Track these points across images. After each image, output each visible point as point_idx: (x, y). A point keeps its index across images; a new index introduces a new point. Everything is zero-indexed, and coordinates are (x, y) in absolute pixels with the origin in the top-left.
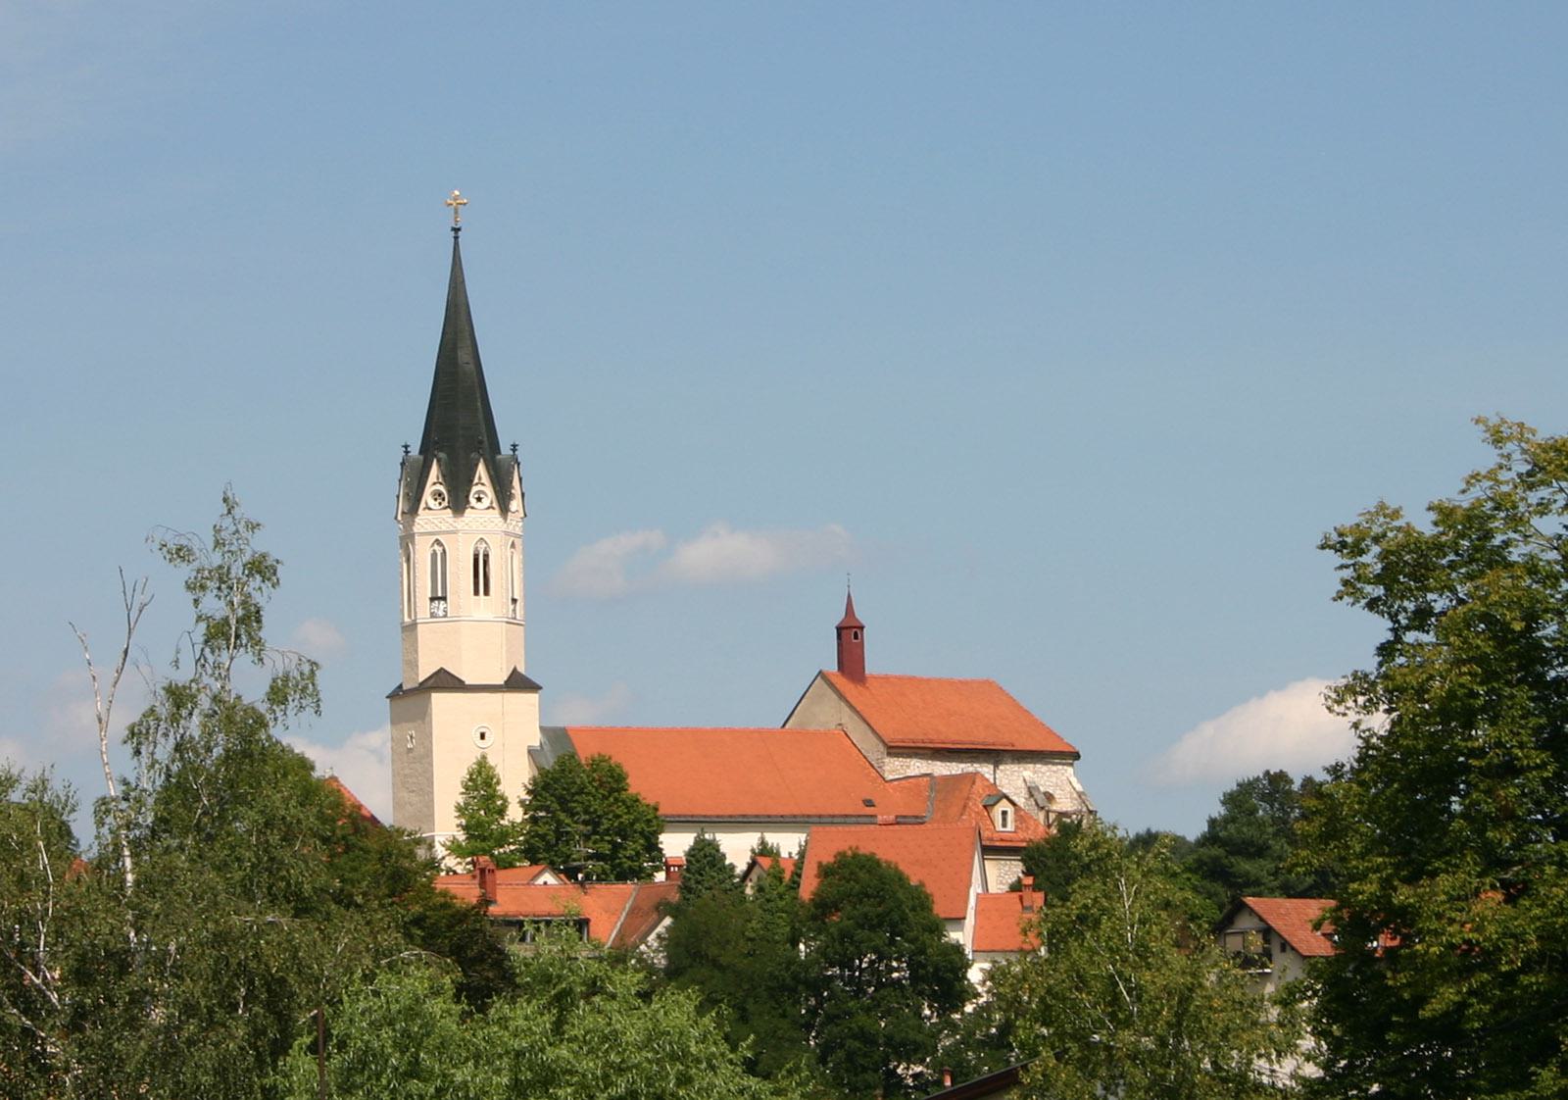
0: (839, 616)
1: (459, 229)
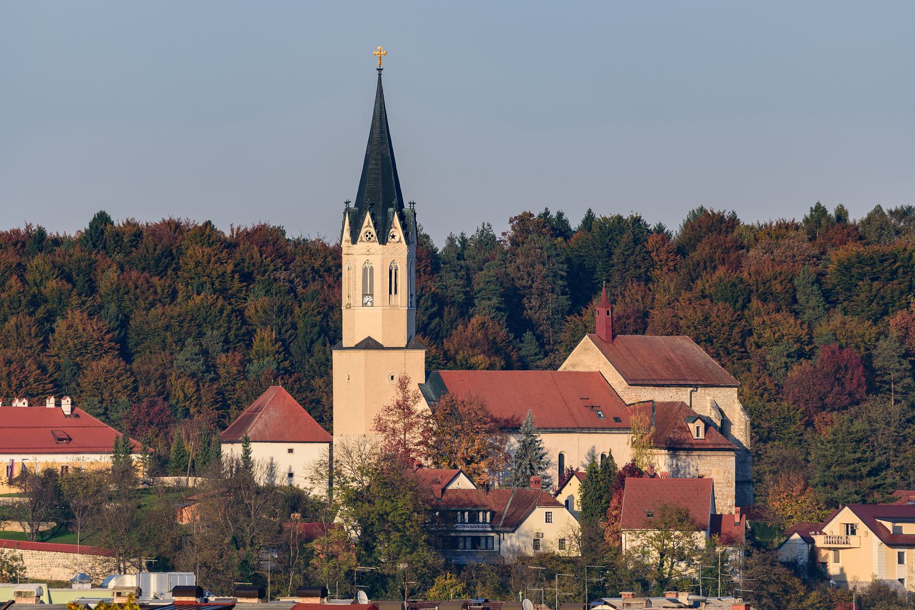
1: (382, 69)
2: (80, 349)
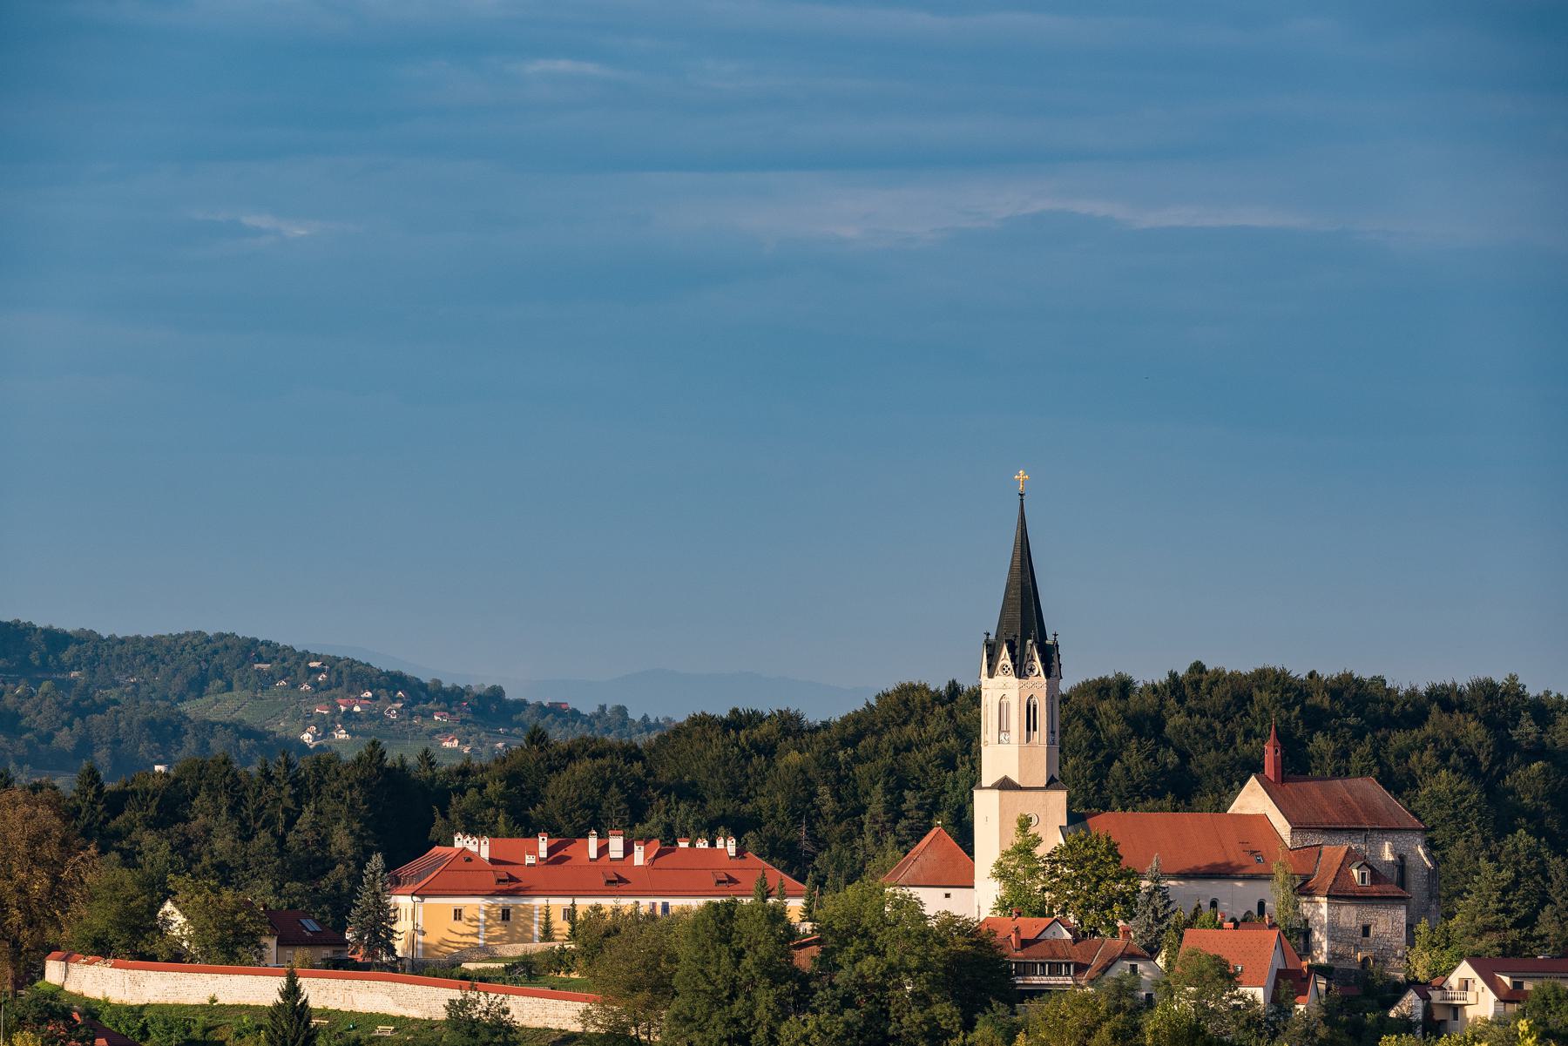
2: (1131, 792)
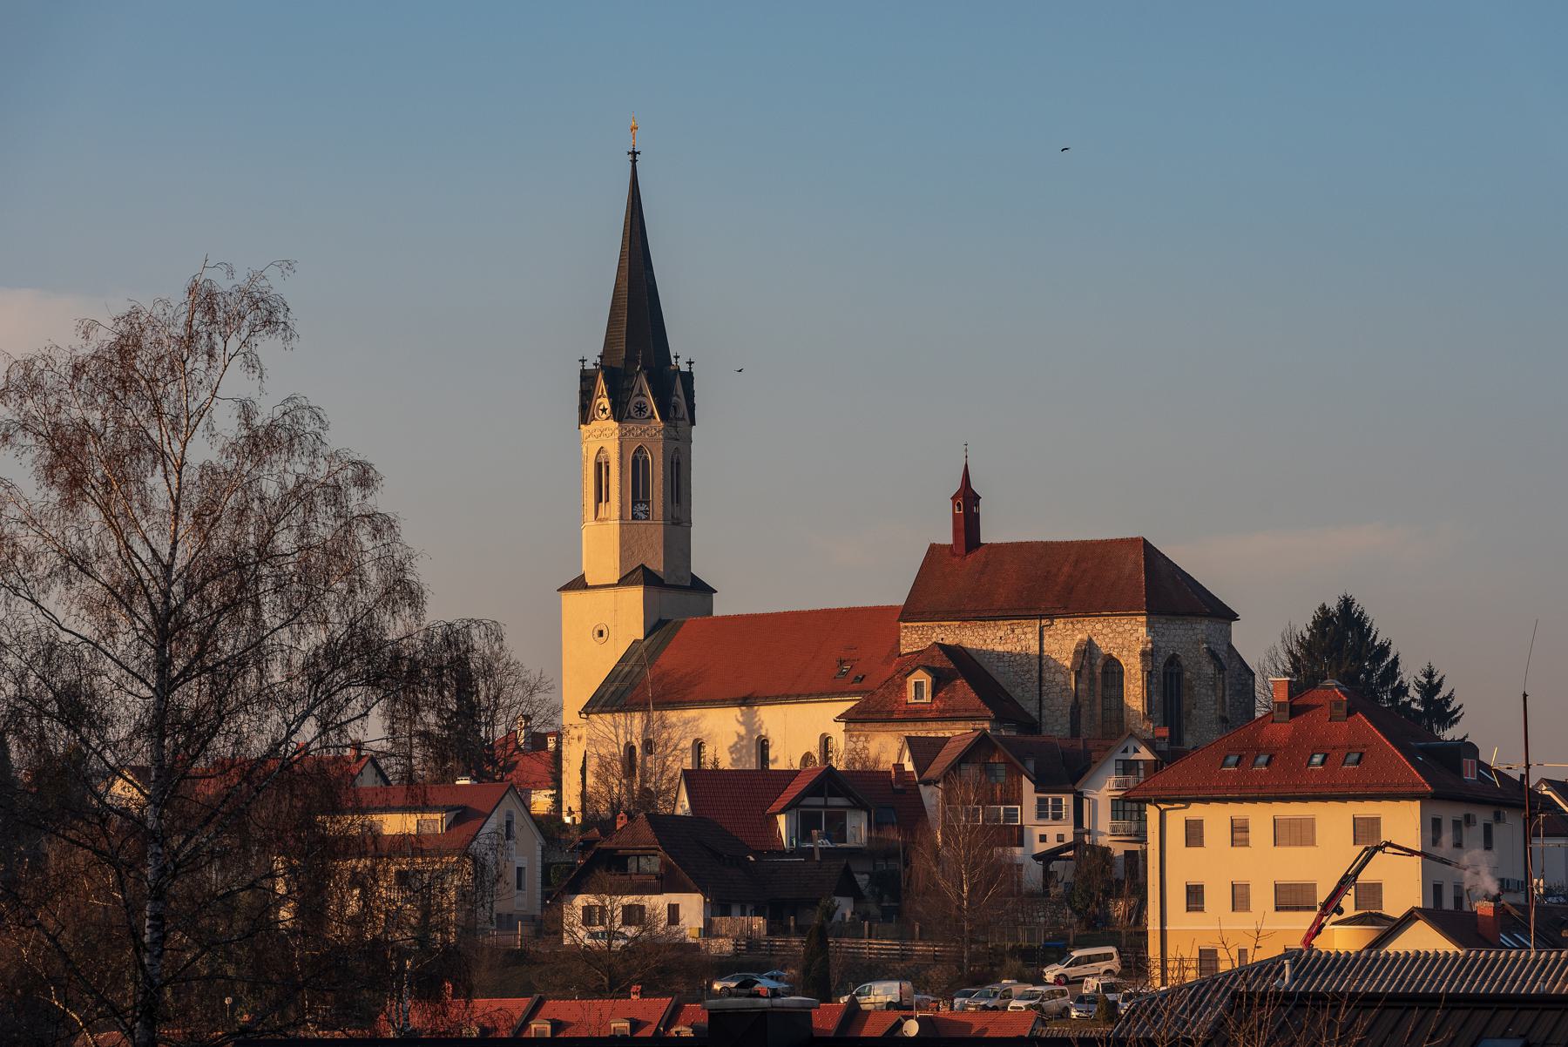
0: (956, 486)
1: (639, 153)
